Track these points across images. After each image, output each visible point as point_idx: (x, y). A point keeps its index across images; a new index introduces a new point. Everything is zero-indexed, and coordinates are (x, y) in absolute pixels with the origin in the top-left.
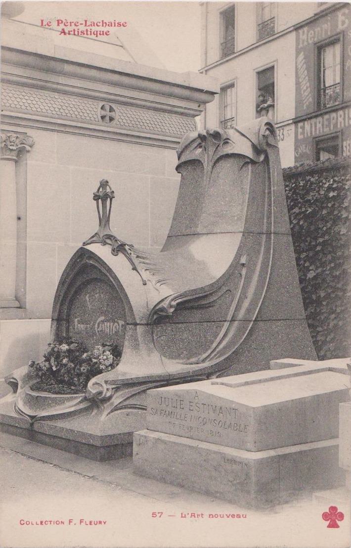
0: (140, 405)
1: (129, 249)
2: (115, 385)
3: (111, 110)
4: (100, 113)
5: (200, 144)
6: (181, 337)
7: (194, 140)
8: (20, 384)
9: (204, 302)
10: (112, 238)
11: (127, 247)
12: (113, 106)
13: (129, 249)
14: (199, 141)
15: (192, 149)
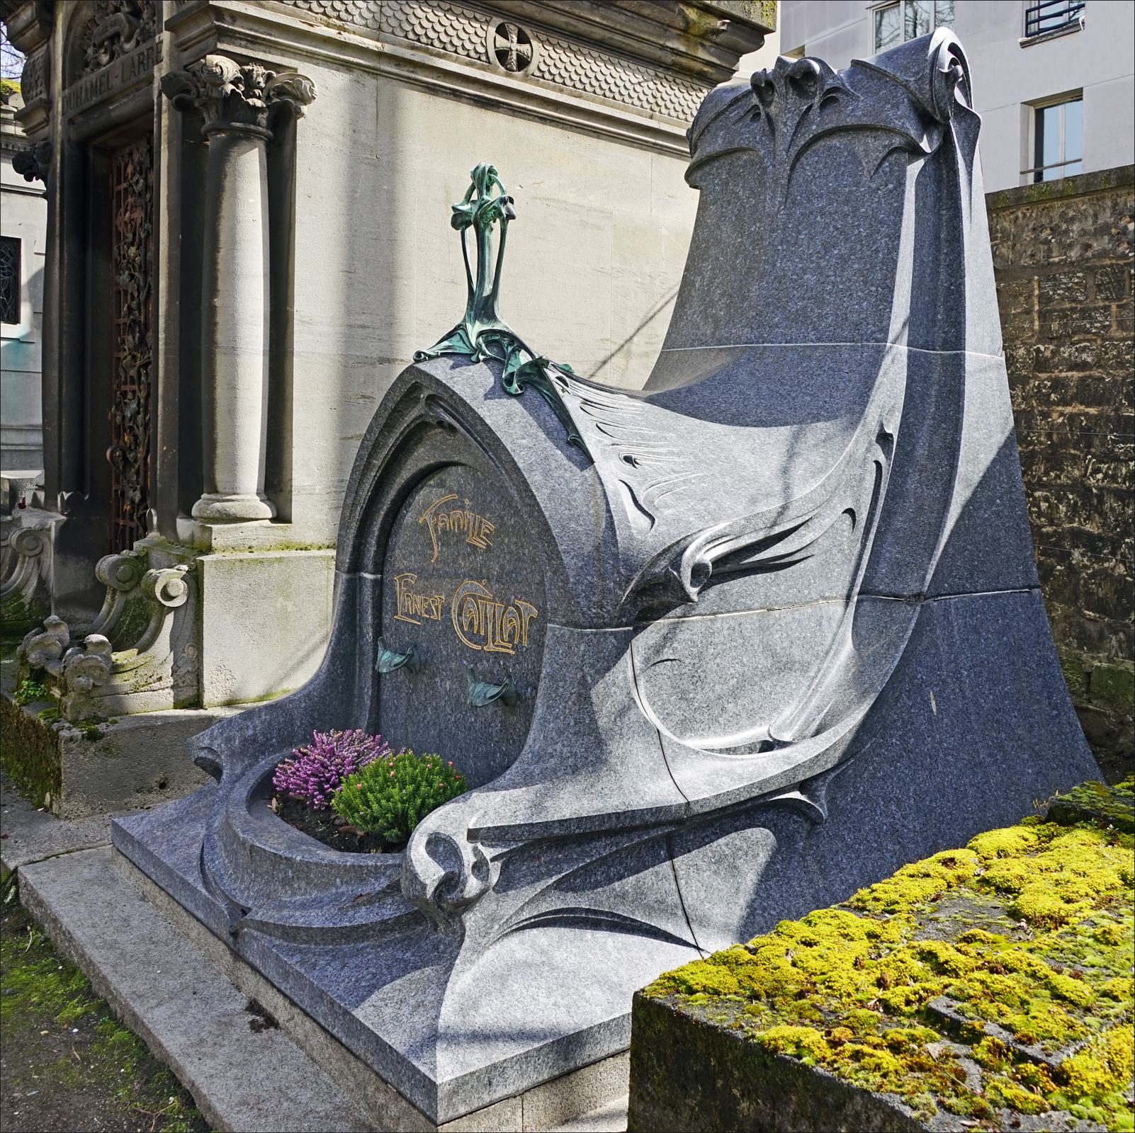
0: (587, 911)
6: (718, 660)
11: (552, 375)
12: (528, 32)
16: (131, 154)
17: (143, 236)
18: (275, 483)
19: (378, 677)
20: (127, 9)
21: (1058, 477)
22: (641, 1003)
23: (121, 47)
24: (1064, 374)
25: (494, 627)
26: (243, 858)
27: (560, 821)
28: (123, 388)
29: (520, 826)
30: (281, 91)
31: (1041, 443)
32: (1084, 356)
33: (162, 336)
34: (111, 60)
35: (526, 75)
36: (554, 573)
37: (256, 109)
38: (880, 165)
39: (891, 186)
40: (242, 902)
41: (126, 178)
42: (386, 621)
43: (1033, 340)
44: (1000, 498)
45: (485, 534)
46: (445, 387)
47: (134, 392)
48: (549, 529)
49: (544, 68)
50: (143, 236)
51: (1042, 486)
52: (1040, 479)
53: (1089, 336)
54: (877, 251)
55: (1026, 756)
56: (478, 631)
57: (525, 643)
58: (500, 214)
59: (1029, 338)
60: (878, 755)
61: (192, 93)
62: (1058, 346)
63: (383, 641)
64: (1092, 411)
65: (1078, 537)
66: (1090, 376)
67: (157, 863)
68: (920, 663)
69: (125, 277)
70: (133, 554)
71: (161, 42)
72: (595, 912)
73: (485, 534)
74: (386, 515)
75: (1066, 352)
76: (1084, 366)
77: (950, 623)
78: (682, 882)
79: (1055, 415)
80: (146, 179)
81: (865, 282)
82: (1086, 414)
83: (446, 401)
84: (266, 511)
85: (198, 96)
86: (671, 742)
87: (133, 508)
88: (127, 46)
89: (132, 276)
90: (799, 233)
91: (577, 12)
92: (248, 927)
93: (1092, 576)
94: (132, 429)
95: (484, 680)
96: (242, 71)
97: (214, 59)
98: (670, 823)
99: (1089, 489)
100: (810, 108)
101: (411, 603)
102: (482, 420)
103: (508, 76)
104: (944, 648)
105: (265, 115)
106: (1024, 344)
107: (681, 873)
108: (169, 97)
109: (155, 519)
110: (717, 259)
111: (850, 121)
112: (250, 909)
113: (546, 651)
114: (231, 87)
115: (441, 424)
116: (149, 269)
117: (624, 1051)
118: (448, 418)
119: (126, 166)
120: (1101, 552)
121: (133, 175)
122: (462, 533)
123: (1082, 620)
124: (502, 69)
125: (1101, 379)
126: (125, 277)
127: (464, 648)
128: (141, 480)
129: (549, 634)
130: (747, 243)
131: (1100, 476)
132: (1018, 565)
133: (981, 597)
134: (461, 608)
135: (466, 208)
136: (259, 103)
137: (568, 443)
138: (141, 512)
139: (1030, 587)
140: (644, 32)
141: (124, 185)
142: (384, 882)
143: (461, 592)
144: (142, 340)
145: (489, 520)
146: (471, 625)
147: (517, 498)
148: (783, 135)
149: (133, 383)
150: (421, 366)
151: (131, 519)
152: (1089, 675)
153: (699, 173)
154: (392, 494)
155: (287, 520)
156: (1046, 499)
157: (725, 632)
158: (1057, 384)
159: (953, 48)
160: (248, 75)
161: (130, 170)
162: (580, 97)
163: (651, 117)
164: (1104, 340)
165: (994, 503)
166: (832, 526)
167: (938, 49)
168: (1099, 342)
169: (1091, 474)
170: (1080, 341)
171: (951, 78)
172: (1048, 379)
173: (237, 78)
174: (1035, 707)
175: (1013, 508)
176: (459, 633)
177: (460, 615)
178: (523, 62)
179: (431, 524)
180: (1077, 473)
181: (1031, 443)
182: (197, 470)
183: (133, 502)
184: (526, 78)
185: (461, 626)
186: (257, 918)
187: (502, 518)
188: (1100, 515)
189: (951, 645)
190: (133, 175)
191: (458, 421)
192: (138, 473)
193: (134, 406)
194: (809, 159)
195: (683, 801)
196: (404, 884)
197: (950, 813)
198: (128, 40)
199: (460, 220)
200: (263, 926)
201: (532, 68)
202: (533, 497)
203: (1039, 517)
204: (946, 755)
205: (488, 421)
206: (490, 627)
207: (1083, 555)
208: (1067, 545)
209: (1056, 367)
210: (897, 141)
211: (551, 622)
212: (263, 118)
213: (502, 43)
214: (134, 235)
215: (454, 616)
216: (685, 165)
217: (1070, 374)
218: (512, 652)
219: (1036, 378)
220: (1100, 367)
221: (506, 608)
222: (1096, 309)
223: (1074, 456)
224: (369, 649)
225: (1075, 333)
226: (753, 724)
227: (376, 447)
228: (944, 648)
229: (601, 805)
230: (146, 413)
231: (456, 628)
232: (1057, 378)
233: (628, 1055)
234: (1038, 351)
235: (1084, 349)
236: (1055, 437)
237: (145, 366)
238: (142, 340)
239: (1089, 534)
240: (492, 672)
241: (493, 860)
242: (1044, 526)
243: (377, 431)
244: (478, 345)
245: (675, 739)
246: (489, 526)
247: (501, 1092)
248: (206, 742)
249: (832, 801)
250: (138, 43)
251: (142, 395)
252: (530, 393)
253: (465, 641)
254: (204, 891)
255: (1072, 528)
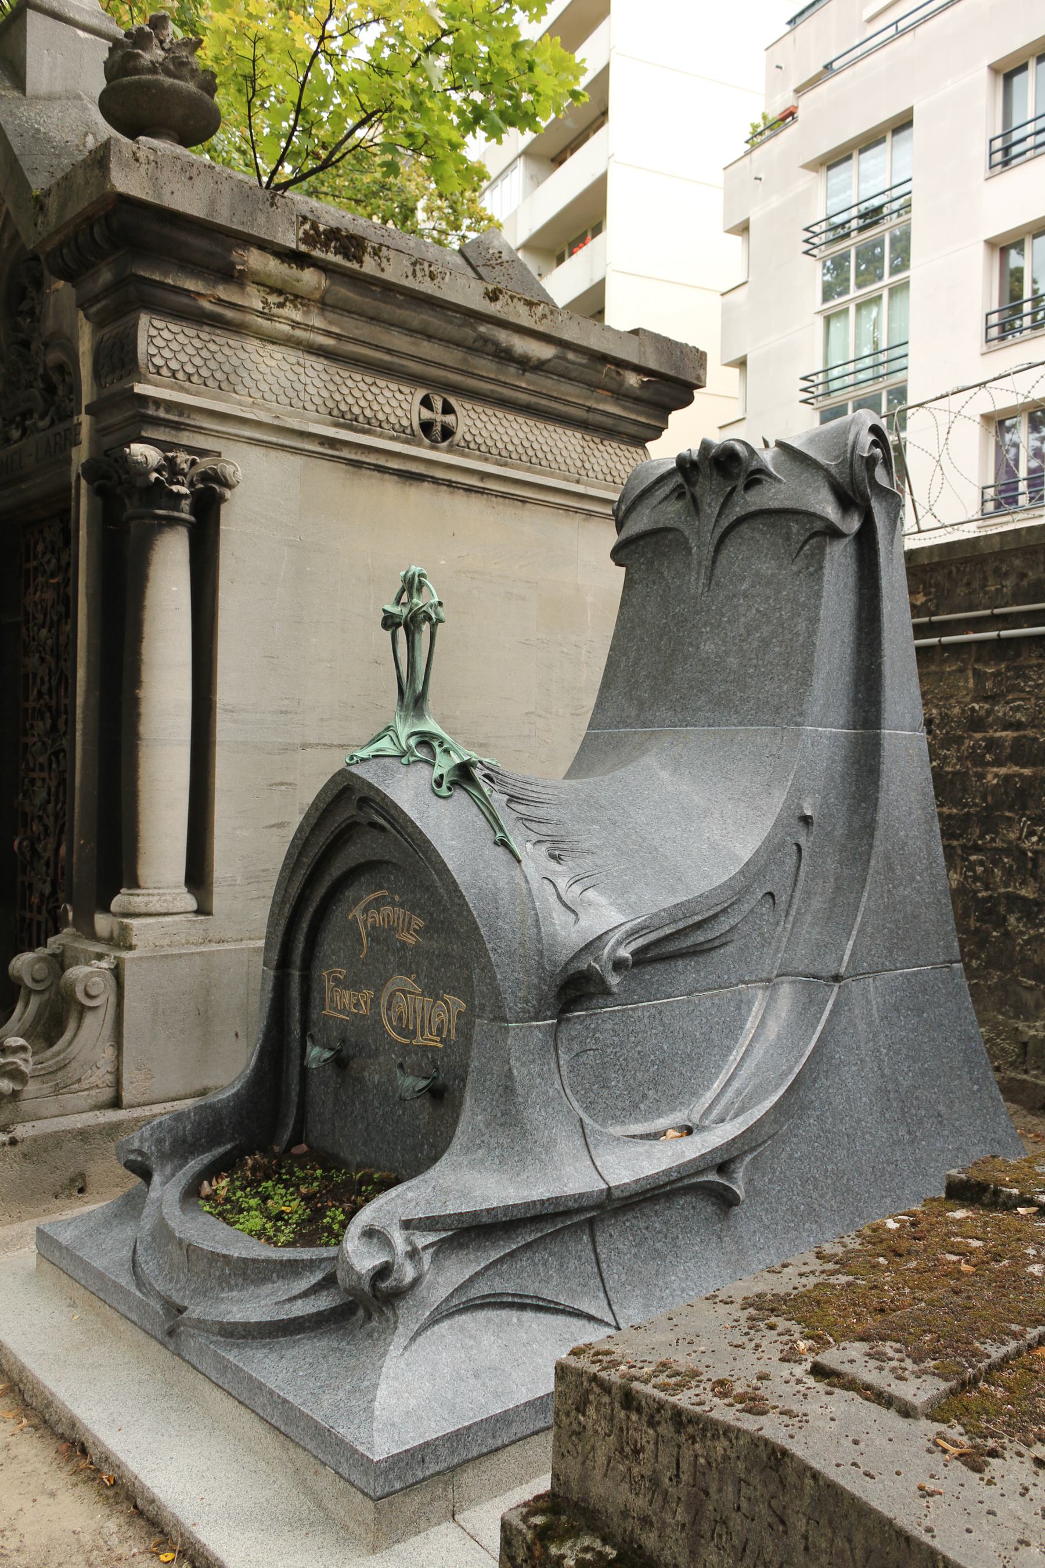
0: (514, 1295)
1: (485, 776)
2: (445, 1230)
3: (448, 409)
4: (417, 414)
5: (680, 486)
6: (639, 1048)
7: (662, 479)
8: (154, 1162)
9: (700, 937)
10: (436, 744)
11: (478, 774)
12: (453, 401)
13: (485, 776)
14: (679, 479)
15: (655, 502)
16: (41, 532)
17: (55, 618)
18: (198, 873)
19: (304, 1071)
20: (41, 386)
21: (993, 840)
22: (562, 1371)
23: (34, 424)
24: (998, 734)
25: (422, 1021)
26: (178, 1256)
27: (488, 1210)
28: (32, 775)
29: (450, 1215)
30: (205, 477)
31: (975, 805)
32: (1018, 715)
33: (79, 726)
34: (21, 438)
35: (451, 446)
36: (482, 970)
37: (180, 496)
38: (802, 548)
39: (812, 569)
40: (178, 1301)
41: (36, 557)
42: (314, 1016)
43: (968, 699)
44: (920, 874)
45: (415, 930)
46: (377, 790)
47: (43, 780)
48: (477, 928)
49: (468, 437)
50: (55, 618)
51: (977, 849)
52: (975, 841)
53: (1023, 695)
54: (798, 634)
55: (946, 1133)
56: (407, 1025)
57: (453, 1037)
58: (430, 618)
59: (964, 696)
60: (796, 1136)
61: (113, 476)
62: (993, 705)
63: (312, 1036)
64: (1027, 772)
65: (1013, 900)
66: (1025, 736)
67: (87, 1267)
68: (837, 1043)
69: (35, 659)
70: (47, 951)
71: (80, 424)
72: (521, 1296)
73: (415, 930)
74: (316, 912)
75: (1000, 710)
76: (1018, 726)
77: (868, 1002)
78: (604, 1266)
79: (990, 777)
80: (59, 560)
81: (787, 665)
82: (1020, 775)
83: (377, 803)
84: (190, 902)
85: (120, 483)
86: (594, 1132)
87: (42, 901)
88: (41, 424)
89: (42, 660)
90: (723, 615)
91: (502, 378)
92: (185, 1325)
93: (1027, 942)
94: (40, 818)
95: (412, 1073)
96: (166, 458)
97: (138, 450)
98: (592, 1208)
99: (1024, 853)
100: (733, 490)
101: (341, 1002)
102: (412, 822)
103: (433, 448)
104: (862, 1027)
105: (188, 502)
106: (959, 702)
107: (602, 1257)
108: (90, 482)
109: (71, 915)
110: (642, 640)
111: (774, 504)
112: (186, 1308)
113: (474, 1045)
114: (155, 475)
115: (373, 825)
116: (65, 651)
117: (548, 1428)
118: (381, 821)
119: (36, 543)
120: (1036, 917)
121: (44, 554)
122: (392, 929)
123: (1019, 989)
124: (427, 441)
125: (1036, 739)
126: (35, 659)
127: (393, 1042)
128: (51, 871)
129: (477, 1029)
130: (672, 625)
131: (1034, 839)
132: (939, 940)
133: (901, 975)
134: (390, 1004)
135: (395, 610)
136: (184, 490)
137: (495, 843)
138: (51, 905)
139: (952, 962)
140: (571, 395)
141: (35, 563)
142: (319, 1276)
143: (390, 987)
144: (54, 728)
145: (419, 916)
146: (400, 1019)
147: (446, 897)
148: (709, 515)
149: (42, 769)
150: (354, 769)
151: (39, 912)
152: (1025, 1045)
153: (624, 553)
154: (321, 891)
155: (209, 913)
156: (981, 863)
157: (646, 1021)
158: (992, 744)
159: (875, 430)
160: (171, 462)
161: (40, 548)
162: (505, 465)
163: (578, 482)
164: (1038, 698)
165: (914, 879)
166: (752, 911)
167: (857, 434)
168: (1033, 701)
169: (1026, 837)
170: (1014, 700)
171: (870, 463)
172: (984, 739)
173: (162, 466)
174: (956, 1082)
175: (934, 883)
176: (388, 1027)
177: (388, 1009)
178: (447, 433)
179: (360, 918)
180: (1012, 836)
181: (966, 805)
182: (117, 863)
183: (42, 895)
184: (450, 450)
185: (390, 1021)
186: (195, 1316)
187: (431, 914)
188: (1035, 879)
189: (870, 1024)
190: (44, 554)
191: (389, 822)
192: (47, 864)
193: (43, 795)
194: (730, 551)
195: (604, 1186)
196: (340, 1275)
197: (868, 1192)
198: (42, 417)
199: (389, 622)
200: (200, 1324)
201: (458, 437)
202: (462, 897)
203: (974, 882)
204: (864, 1134)
205: (418, 824)
206: (419, 1021)
207: (1018, 920)
208: (1002, 910)
209: (991, 726)
210: (818, 526)
211: (479, 1017)
212: (185, 504)
213: (426, 414)
214: (45, 615)
215: (383, 1010)
216: (610, 537)
217: (1004, 734)
218: (441, 1046)
219: (971, 738)
220: (1034, 727)
221: (435, 1002)
222: (1030, 667)
223: (1009, 819)
224: (296, 1045)
225: (1009, 691)
226: (673, 1110)
227: (306, 843)
228: (862, 1027)
229: (526, 1193)
230: (57, 802)
231: (385, 1022)
232: (992, 739)
233: (551, 1436)
234: (973, 709)
235: (1018, 709)
236: (989, 799)
237: (56, 754)
238: (54, 728)
239: (1024, 899)
240: (420, 1066)
241: (425, 1248)
242: (980, 891)
243: (308, 830)
244: (409, 747)
245: (598, 1127)
246: (419, 922)
247: (434, 1468)
248: (136, 1145)
249: (750, 1182)
250: (52, 423)
251: (53, 784)
252: (459, 794)
253: (394, 1035)
254: (138, 1293)
255: (1008, 893)
